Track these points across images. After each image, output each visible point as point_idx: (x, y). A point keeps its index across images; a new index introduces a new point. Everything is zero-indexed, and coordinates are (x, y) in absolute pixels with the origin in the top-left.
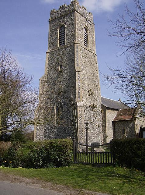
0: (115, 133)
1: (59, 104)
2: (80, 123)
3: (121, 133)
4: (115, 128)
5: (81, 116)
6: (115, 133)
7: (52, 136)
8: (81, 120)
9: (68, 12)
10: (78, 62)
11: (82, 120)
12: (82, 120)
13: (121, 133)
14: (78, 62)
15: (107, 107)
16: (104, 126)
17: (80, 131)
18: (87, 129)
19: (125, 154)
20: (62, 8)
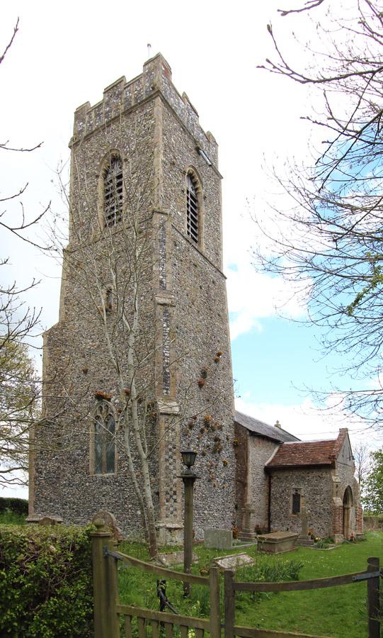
0: (270, 502)
1: (104, 410)
2: (167, 468)
3: (287, 503)
4: (270, 490)
5: (170, 447)
6: (270, 502)
7: (84, 504)
8: (171, 457)
9: (133, 104)
10: (165, 276)
11: (175, 460)
12: (175, 457)
13: (287, 503)
14: (165, 276)
15: (250, 431)
16: (241, 483)
17: (175, 501)
18: (189, 481)
19: (21, 552)
20: (114, 90)
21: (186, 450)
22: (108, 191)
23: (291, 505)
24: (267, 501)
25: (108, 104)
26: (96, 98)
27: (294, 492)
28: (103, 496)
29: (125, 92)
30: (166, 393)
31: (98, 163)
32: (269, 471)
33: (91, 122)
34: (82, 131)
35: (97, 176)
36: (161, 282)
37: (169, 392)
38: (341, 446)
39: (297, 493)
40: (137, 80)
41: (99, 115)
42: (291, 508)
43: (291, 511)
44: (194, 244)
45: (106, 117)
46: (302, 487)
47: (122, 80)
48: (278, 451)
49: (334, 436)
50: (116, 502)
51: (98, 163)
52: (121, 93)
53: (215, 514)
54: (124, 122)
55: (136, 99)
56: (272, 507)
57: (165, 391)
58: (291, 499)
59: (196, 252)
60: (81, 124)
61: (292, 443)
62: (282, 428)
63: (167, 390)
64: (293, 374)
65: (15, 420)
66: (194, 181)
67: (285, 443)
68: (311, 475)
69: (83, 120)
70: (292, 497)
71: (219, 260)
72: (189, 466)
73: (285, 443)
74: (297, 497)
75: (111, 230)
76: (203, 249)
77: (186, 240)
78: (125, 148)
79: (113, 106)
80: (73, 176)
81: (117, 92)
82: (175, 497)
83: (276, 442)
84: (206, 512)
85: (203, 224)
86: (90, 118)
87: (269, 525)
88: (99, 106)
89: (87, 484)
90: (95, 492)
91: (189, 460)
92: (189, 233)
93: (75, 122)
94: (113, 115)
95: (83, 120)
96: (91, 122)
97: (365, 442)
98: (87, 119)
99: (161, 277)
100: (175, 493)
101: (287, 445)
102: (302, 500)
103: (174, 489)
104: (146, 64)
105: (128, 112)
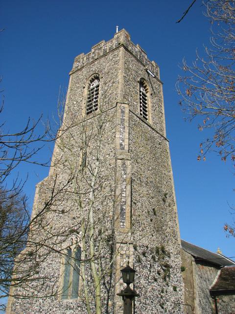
21: (118, 238)
22: (90, 91)
30: (123, 225)
32: (215, 293)
35: (84, 88)
36: (121, 145)
37: (125, 224)
44: (145, 120)
52: (101, 48)
54: (103, 59)
55: (110, 49)
57: (122, 224)
63: (123, 222)
65: (216, 306)
75: (91, 115)
77: (139, 118)
86: (83, 60)
91: (128, 278)
92: (141, 114)
94: (96, 57)
97: (6, 313)
99: (121, 141)
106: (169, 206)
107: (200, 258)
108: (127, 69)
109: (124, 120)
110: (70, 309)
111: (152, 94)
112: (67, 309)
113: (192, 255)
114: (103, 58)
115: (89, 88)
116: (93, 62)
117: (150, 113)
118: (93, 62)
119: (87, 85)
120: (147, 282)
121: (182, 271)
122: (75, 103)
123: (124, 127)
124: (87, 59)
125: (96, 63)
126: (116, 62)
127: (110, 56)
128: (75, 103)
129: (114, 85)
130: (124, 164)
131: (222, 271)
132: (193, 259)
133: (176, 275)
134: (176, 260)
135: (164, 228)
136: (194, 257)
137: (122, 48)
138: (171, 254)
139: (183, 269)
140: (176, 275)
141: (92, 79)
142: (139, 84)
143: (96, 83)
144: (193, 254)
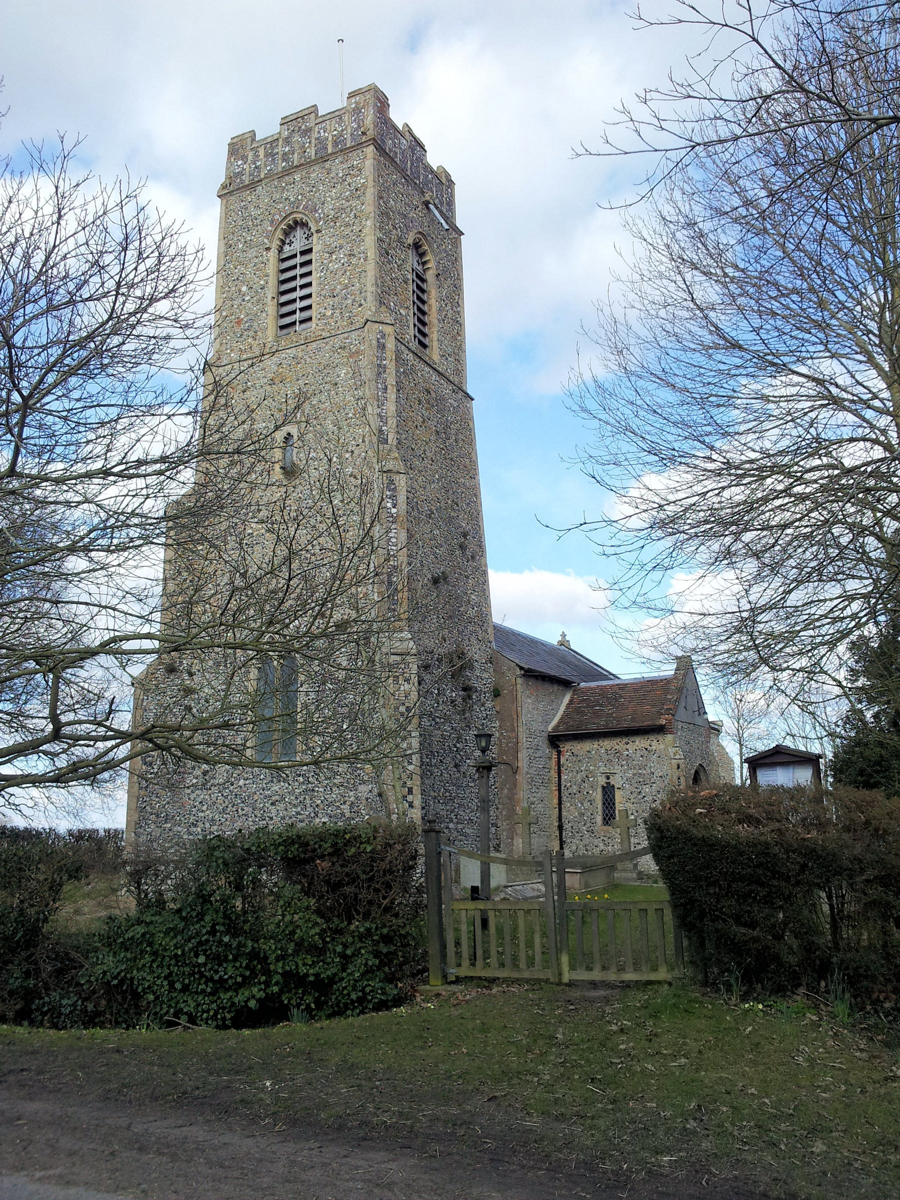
23: (600, 806)
24: (547, 685)
25: (287, 141)
26: (268, 127)
27: (602, 781)
28: (272, 804)
29: (316, 129)
31: (270, 228)
33: (258, 163)
34: (240, 174)
35: (268, 249)
38: (680, 690)
39: (608, 783)
40: (337, 115)
41: (272, 155)
42: (600, 813)
43: (599, 819)
45: (284, 160)
46: (617, 769)
47: (314, 109)
48: (571, 702)
49: (668, 670)
50: (298, 813)
51: (270, 228)
52: (310, 130)
53: (468, 831)
54: (316, 173)
56: (564, 813)
58: (598, 796)
59: (427, 369)
60: (240, 163)
61: (593, 684)
62: (572, 647)
64: (586, 570)
66: (421, 251)
67: (583, 685)
68: (631, 747)
69: (244, 158)
70: (600, 790)
71: (460, 371)
72: (483, 751)
73: (583, 685)
74: (608, 791)
76: (436, 357)
78: (316, 211)
79: (296, 146)
80: (223, 242)
81: (303, 127)
82: (410, 798)
83: (566, 684)
84: (451, 825)
85: (433, 318)
87: (562, 848)
88: (273, 142)
89: (242, 782)
90: (256, 797)
91: (483, 744)
93: (229, 159)
94: (296, 159)
95: (244, 158)
96: (258, 163)
98: (250, 158)
100: (410, 791)
101: (586, 688)
102: (618, 795)
103: (409, 784)
104: (351, 95)
105: (323, 158)
106: (473, 557)
107: (538, 672)
108: (384, 214)
109: (385, 367)
110: (279, 781)
111: (438, 275)
112: (272, 781)
113: (517, 665)
114: (316, 168)
115: (281, 250)
116: (287, 172)
117: (435, 329)
118: (287, 172)
119: (276, 243)
120: (433, 723)
121: (495, 696)
122: (244, 289)
123: (386, 389)
124: (266, 155)
125: (297, 177)
126: (358, 192)
127: (338, 167)
128: (244, 289)
129: (354, 261)
130: (392, 482)
131: (568, 952)
132: (518, 672)
133: (483, 705)
134: (486, 675)
135: (462, 609)
136: (521, 668)
137: (370, 150)
138: (475, 664)
139: (496, 694)
140: (483, 705)
141: (290, 226)
142: (410, 252)
143: (298, 242)
144: (517, 661)
